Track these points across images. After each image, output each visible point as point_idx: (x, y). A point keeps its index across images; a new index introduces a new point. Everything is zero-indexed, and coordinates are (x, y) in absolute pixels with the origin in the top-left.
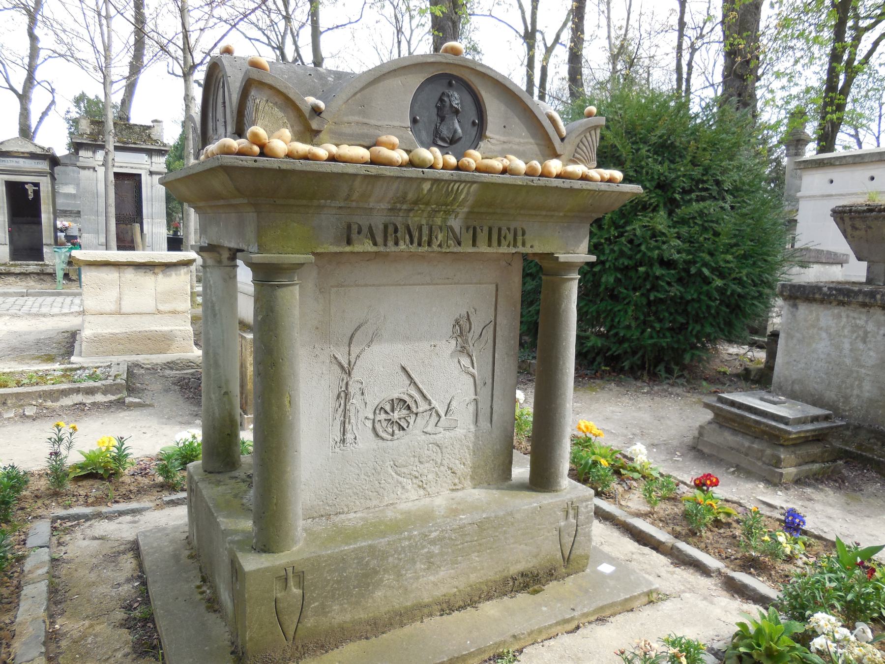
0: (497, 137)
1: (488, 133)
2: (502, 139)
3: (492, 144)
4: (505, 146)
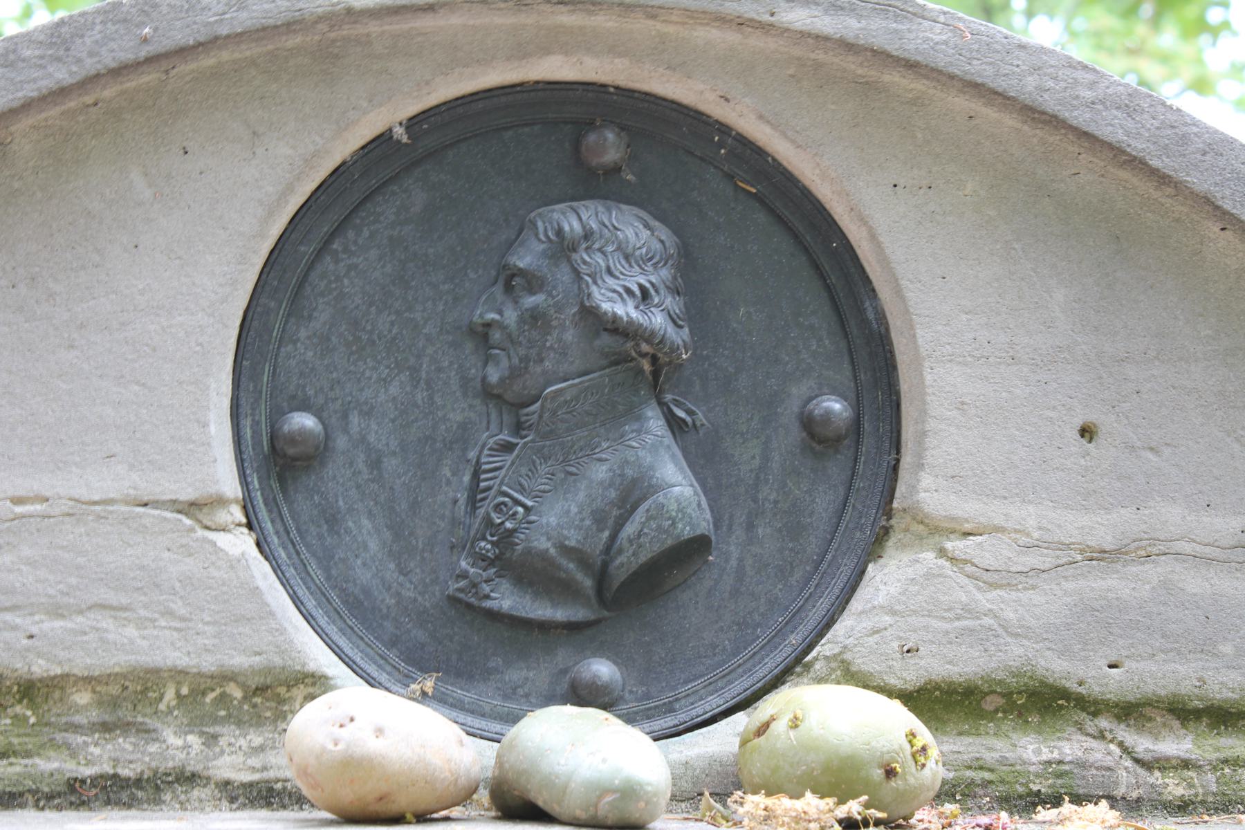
0: (1029, 516)
1: (927, 487)
2: (1102, 528)
3: (989, 578)
4: (1121, 585)
